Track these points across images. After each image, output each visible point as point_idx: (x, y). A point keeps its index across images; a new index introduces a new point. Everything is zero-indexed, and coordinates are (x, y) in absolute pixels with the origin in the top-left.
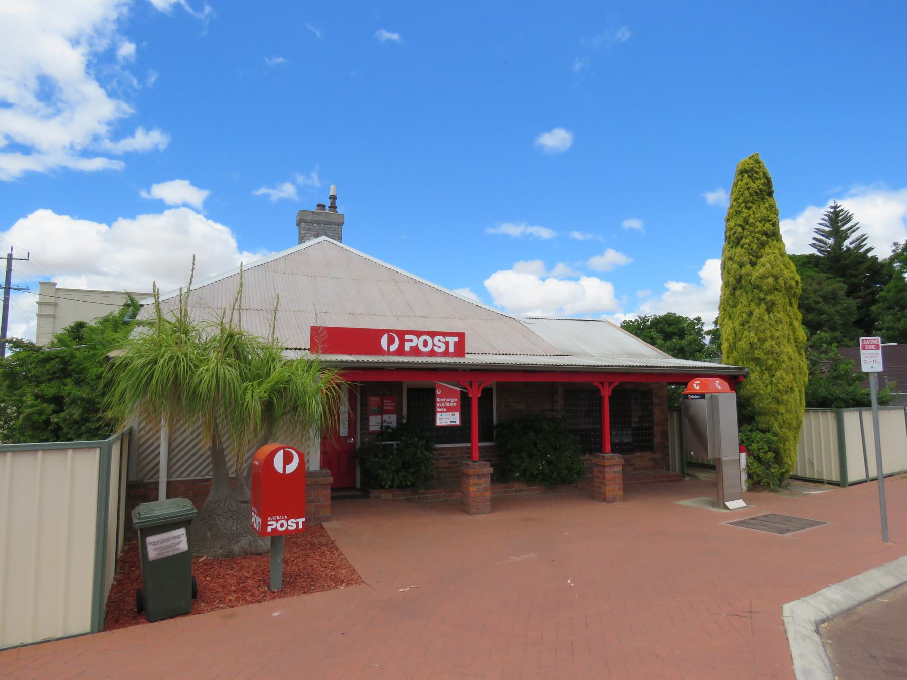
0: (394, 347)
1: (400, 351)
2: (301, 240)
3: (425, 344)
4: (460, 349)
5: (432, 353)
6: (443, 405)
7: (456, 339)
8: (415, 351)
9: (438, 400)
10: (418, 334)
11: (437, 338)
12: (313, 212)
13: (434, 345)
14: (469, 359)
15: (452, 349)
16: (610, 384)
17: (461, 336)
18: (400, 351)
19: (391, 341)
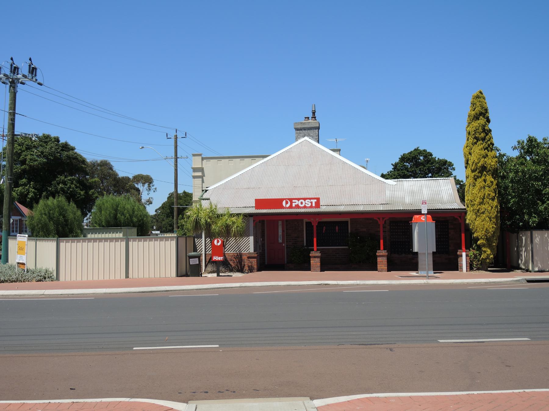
0: (288, 205)
1: (291, 207)
2: (297, 139)
3: (302, 203)
4: (318, 205)
5: (305, 207)
7: (316, 200)
8: (297, 207)
10: (298, 199)
11: (307, 201)
12: (301, 123)
14: (323, 209)
15: (314, 205)
17: (318, 199)
18: (291, 207)
19: (287, 203)
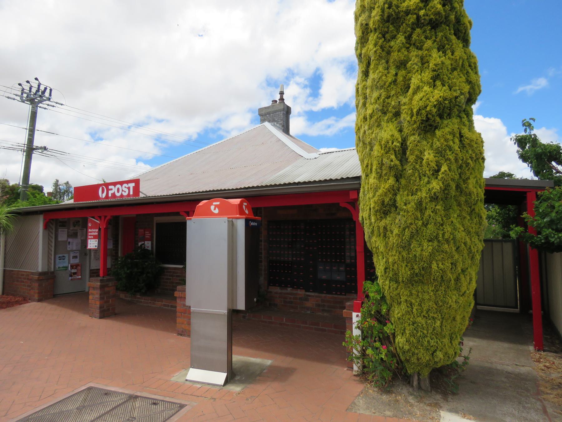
6: (92, 234)
7: (133, 184)
9: (90, 230)
10: (115, 184)
13: (123, 191)
16: (105, 217)
